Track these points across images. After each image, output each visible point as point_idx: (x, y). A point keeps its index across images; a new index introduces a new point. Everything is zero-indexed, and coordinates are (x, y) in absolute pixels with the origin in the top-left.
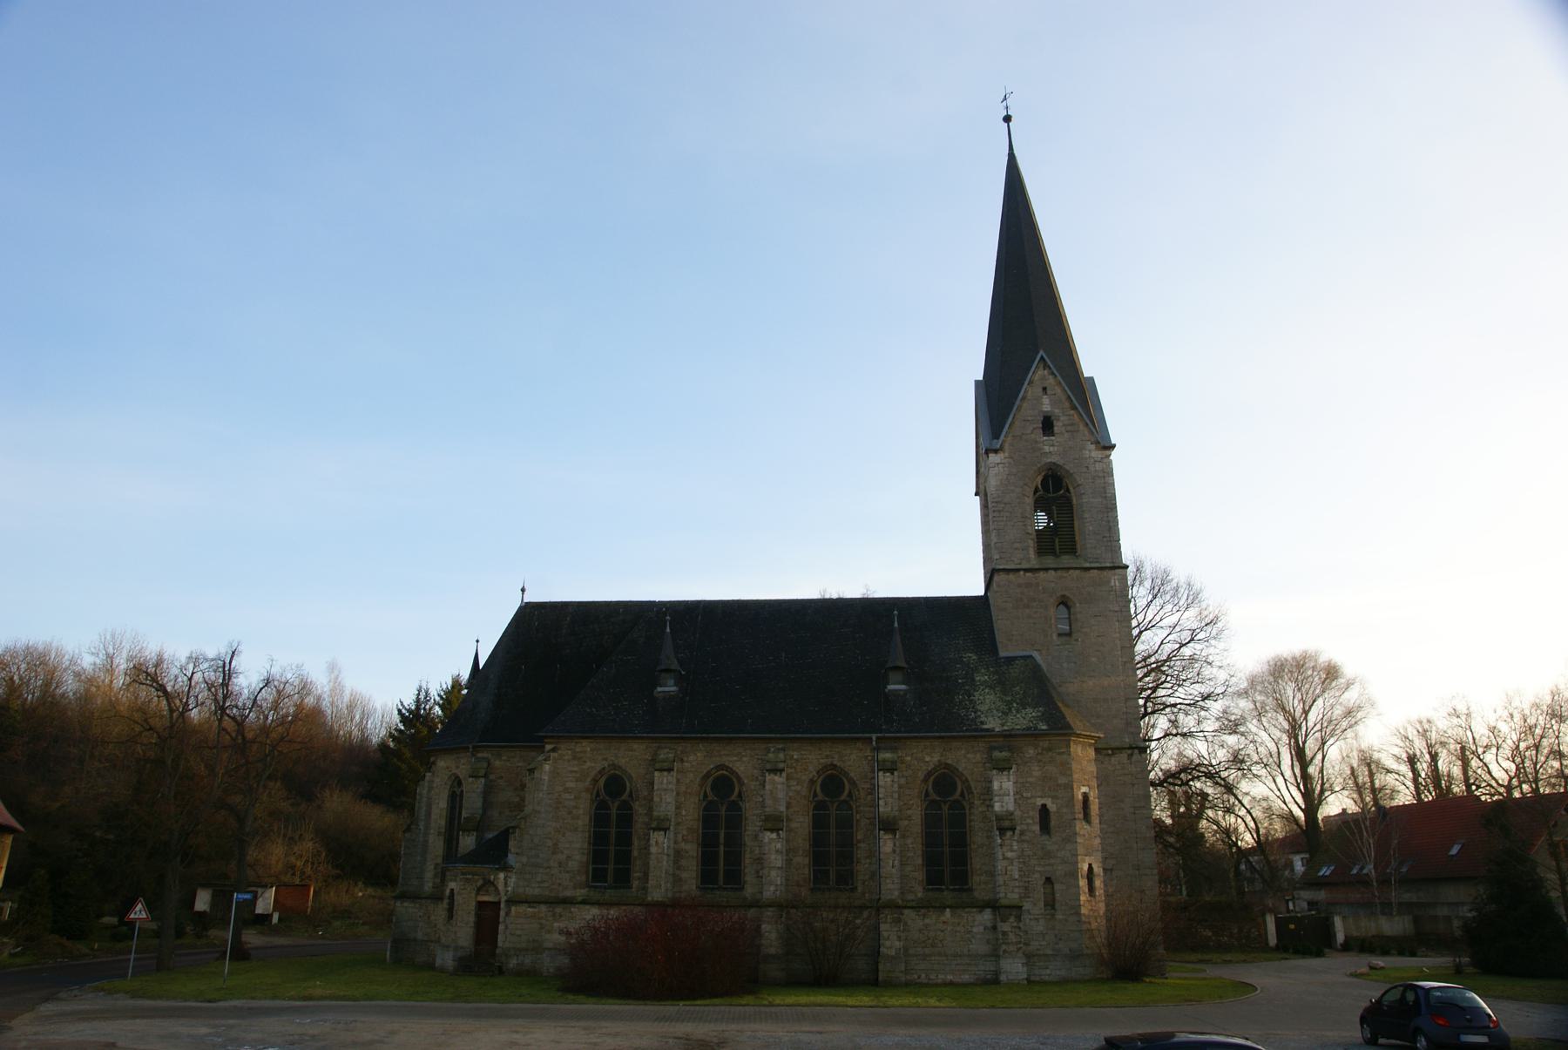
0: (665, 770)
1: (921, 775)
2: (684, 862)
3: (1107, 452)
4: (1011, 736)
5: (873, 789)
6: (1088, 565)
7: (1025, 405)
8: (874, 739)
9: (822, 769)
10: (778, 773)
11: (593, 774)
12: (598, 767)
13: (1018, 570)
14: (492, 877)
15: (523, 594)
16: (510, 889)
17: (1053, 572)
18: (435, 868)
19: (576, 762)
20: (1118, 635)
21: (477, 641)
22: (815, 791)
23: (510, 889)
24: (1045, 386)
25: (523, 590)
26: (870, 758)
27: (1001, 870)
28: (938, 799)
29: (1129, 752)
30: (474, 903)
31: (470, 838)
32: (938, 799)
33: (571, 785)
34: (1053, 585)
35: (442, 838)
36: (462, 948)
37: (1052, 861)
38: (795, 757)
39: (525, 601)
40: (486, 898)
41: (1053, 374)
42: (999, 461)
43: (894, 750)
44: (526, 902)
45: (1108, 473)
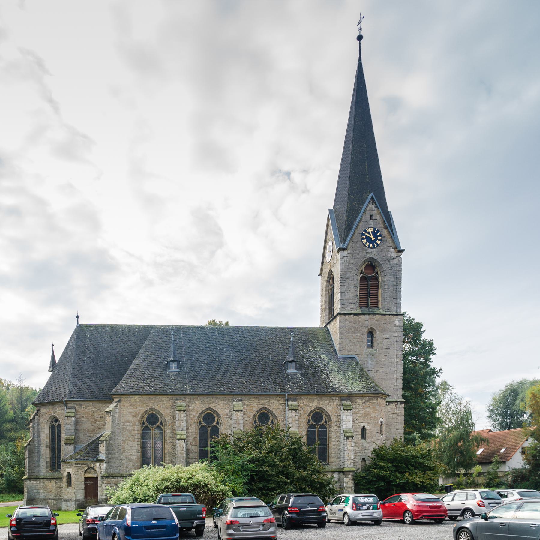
0: (182, 411)
1: (308, 412)
2: (191, 455)
3: (400, 254)
4: (351, 394)
5: (285, 418)
6: (384, 313)
7: (361, 224)
8: (286, 395)
9: (259, 410)
10: (240, 412)
11: (142, 412)
12: (144, 409)
13: (351, 314)
14: (93, 465)
15: (78, 319)
16: (102, 470)
17: (368, 316)
18: (46, 464)
19: (132, 407)
20: (396, 348)
21: (53, 345)
22: (255, 420)
23: (102, 470)
24: (372, 214)
25: (78, 317)
26: (283, 404)
27: (346, 455)
28: (314, 423)
29: (396, 403)
30: (84, 478)
31: (70, 447)
32: (314, 423)
33: (131, 419)
34: (367, 322)
35: (48, 448)
36: (79, 500)
37: (366, 451)
38: (247, 404)
39: (79, 323)
40: (90, 476)
41: (377, 207)
42: (345, 256)
43: (295, 400)
44: (112, 476)
45: (399, 265)
